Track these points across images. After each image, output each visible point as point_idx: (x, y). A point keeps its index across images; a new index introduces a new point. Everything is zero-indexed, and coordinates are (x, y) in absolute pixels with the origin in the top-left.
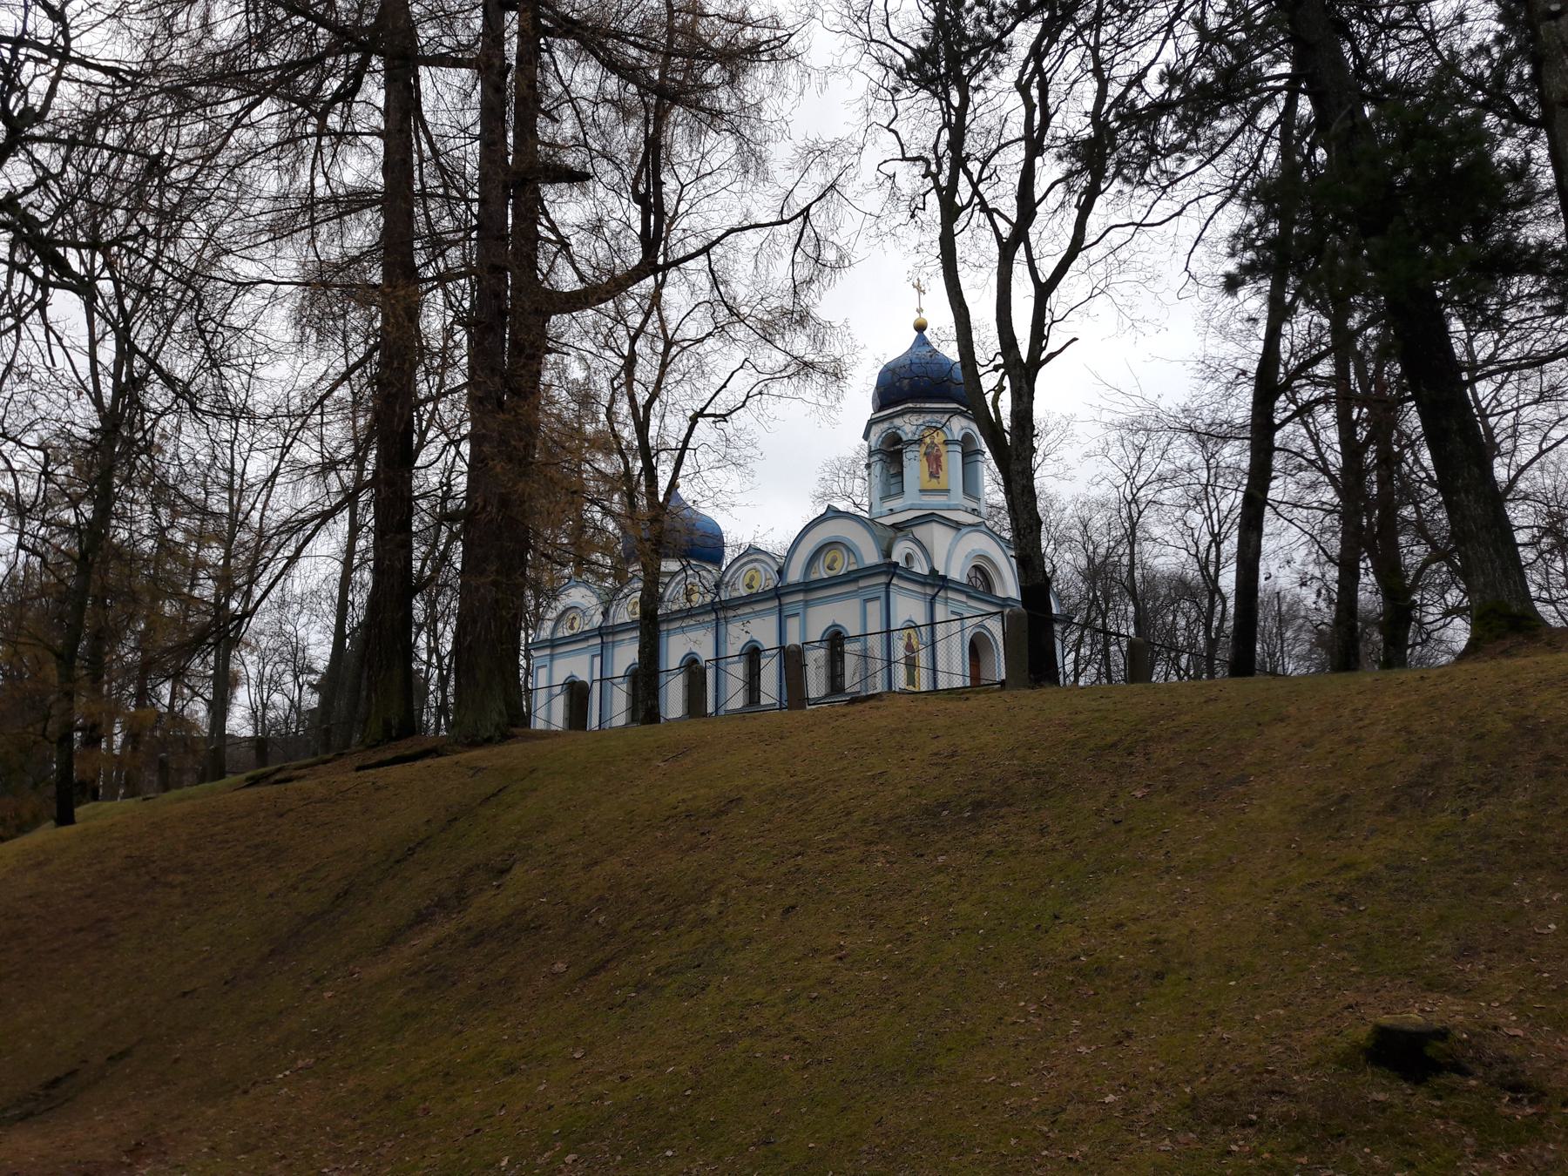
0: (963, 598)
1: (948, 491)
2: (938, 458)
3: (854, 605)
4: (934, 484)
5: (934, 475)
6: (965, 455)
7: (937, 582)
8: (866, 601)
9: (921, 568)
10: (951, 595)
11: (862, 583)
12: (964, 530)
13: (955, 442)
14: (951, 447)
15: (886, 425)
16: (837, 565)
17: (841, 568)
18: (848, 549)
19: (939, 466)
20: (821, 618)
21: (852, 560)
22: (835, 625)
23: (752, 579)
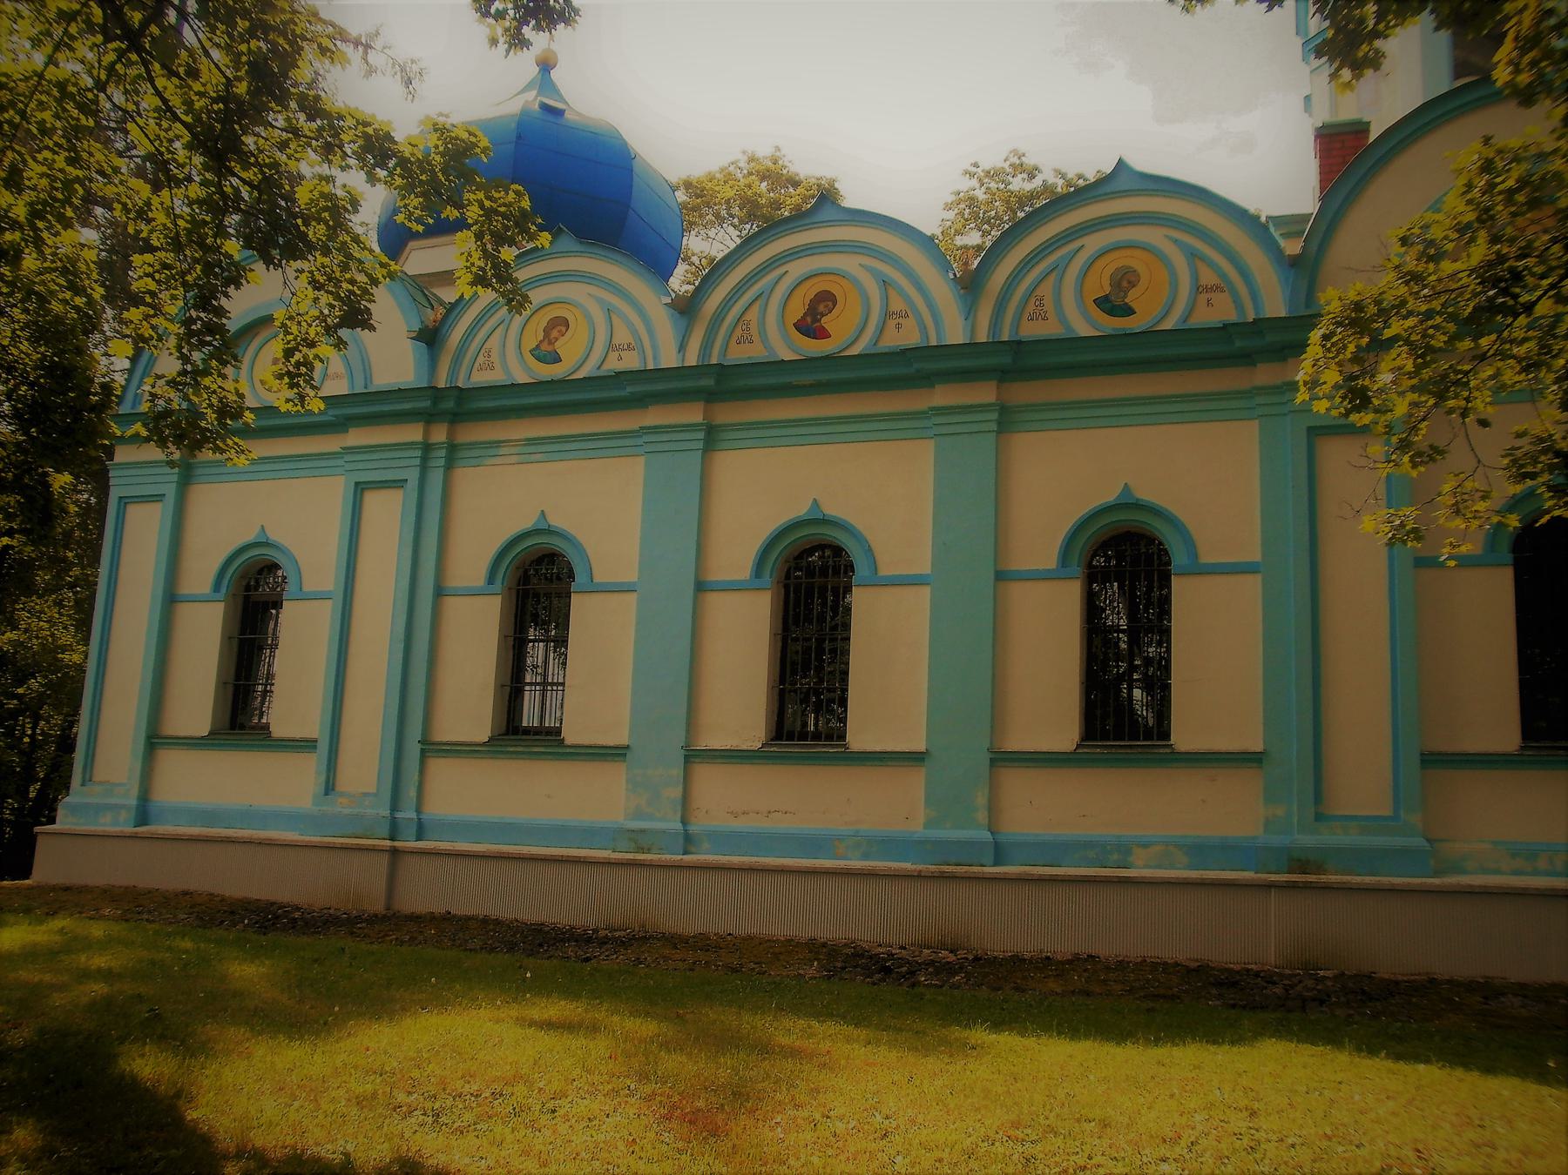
20: (505, 495)
23: (824, 301)
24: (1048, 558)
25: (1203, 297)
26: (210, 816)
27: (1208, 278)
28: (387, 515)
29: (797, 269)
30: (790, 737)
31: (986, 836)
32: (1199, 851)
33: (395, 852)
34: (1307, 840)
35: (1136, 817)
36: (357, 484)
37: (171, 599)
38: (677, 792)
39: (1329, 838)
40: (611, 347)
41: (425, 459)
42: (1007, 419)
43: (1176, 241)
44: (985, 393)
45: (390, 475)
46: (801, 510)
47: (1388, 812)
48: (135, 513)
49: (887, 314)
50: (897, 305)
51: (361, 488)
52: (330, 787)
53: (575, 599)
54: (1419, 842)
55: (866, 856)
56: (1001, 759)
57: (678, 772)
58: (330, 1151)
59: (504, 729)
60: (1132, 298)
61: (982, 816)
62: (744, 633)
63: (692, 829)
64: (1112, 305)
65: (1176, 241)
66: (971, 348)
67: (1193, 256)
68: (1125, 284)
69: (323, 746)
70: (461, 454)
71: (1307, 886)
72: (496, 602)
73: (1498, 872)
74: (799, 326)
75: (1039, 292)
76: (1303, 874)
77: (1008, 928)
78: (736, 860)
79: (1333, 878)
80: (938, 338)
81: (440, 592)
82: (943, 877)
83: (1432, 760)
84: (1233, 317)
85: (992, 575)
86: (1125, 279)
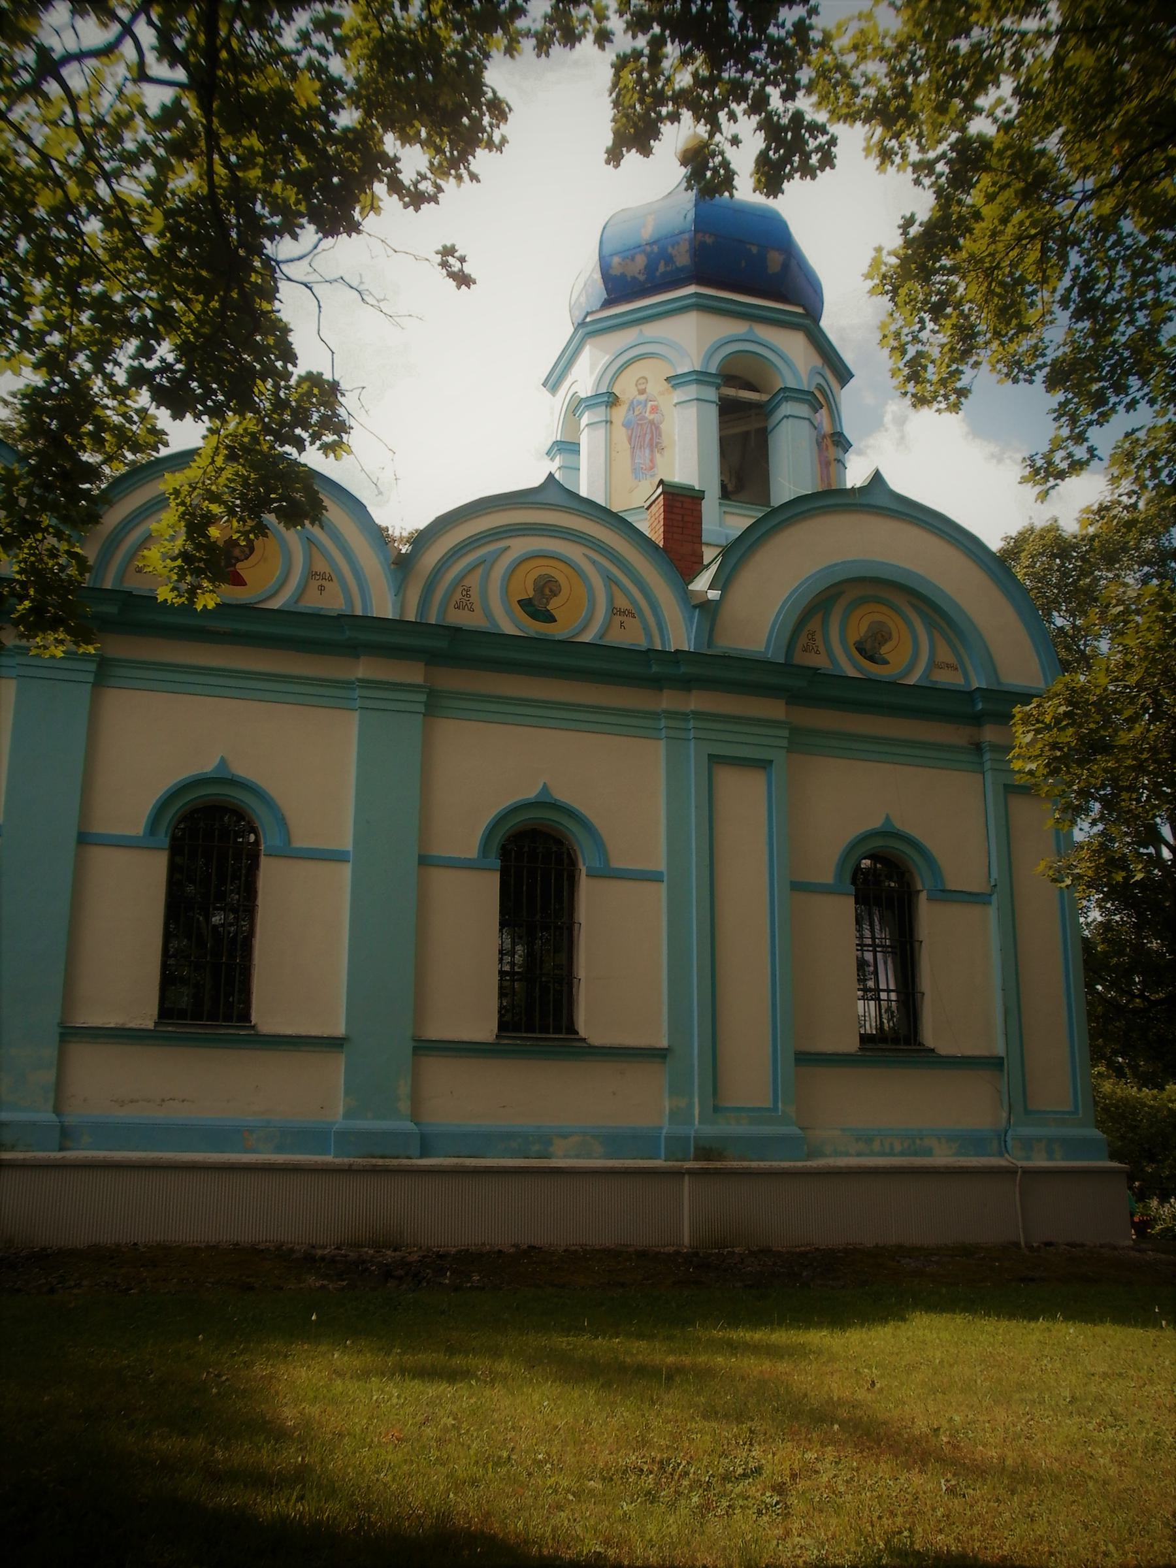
24: (471, 848)
25: (314, 584)
26: (216, 1136)
27: (622, 603)
29: (521, 546)
31: (48, 1116)
32: (615, 1142)
34: (710, 1130)
38: (49, 1076)
42: (435, 704)
43: (594, 562)
44: (414, 673)
46: (207, 766)
47: (769, 1105)
49: (311, 574)
50: (321, 566)
54: (794, 1130)
55: (279, 1149)
56: (424, 1048)
57: (50, 1052)
58: (1006, 1546)
60: (553, 605)
61: (404, 1106)
62: (131, 901)
63: (71, 1120)
64: (535, 609)
65: (594, 562)
66: (397, 625)
67: (610, 580)
68: (547, 591)
71: (718, 1172)
73: (848, 1154)
75: (466, 583)
76: (709, 1161)
79: (735, 1164)
80: (365, 607)
82: (375, 1171)
83: (804, 1059)
84: (643, 644)
85: (74, 834)
86: (547, 587)
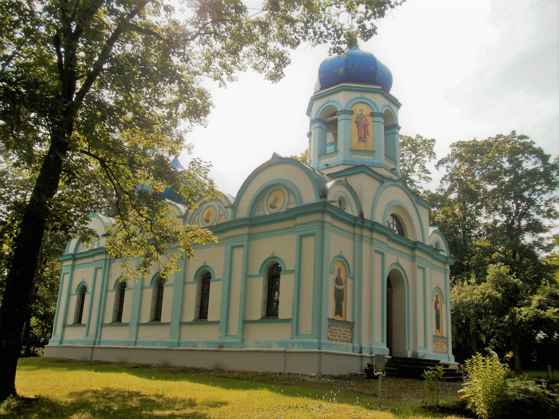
0: (384, 239)
1: (373, 152)
2: (365, 126)
3: (291, 240)
4: (362, 146)
5: (362, 139)
6: (386, 128)
7: (360, 223)
8: (301, 237)
9: (351, 210)
10: (375, 236)
11: (299, 220)
12: (387, 183)
13: (379, 114)
14: (376, 119)
15: (324, 100)
16: (279, 205)
17: (281, 207)
18: (288, 190)
19: (366, 132)
20: (268, 247)
21: (292, 199)
22: (205, 266)
23: (209, 214)
24: (257, 272)
28: (310, 244)
30: (271, 316)
33: (362, 357)
34: (223, 341)
35: (269, 337)
36: (232, 247)
37: (248, 276)
38: (135, 332)
39: (227, 340)
40: (288, 203)
41: (106, 262)
45: (310, 232)
48: (66, 276)
51: (301, 237)
52: (87, 334)
53: (211, 283)
59: (198, 317)
61: (177, 336)
69: (87, 326)
70: (367, 216)
72: (196, 285)
74: (271, 206)
77: (178, 361)
78: (147, 347)
81: (107, 291)
